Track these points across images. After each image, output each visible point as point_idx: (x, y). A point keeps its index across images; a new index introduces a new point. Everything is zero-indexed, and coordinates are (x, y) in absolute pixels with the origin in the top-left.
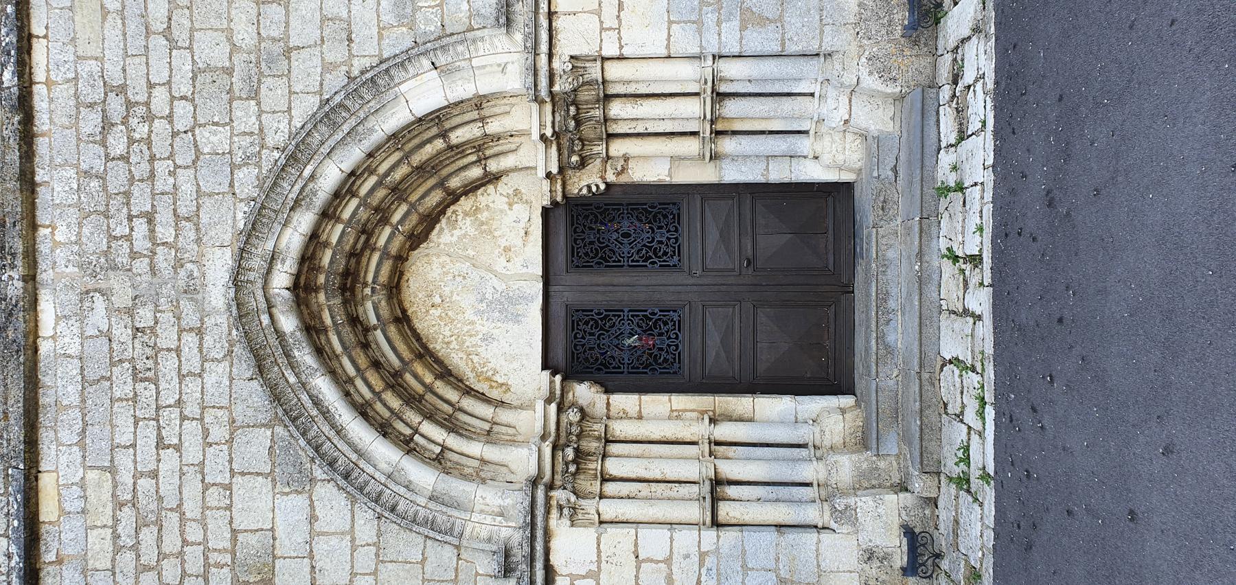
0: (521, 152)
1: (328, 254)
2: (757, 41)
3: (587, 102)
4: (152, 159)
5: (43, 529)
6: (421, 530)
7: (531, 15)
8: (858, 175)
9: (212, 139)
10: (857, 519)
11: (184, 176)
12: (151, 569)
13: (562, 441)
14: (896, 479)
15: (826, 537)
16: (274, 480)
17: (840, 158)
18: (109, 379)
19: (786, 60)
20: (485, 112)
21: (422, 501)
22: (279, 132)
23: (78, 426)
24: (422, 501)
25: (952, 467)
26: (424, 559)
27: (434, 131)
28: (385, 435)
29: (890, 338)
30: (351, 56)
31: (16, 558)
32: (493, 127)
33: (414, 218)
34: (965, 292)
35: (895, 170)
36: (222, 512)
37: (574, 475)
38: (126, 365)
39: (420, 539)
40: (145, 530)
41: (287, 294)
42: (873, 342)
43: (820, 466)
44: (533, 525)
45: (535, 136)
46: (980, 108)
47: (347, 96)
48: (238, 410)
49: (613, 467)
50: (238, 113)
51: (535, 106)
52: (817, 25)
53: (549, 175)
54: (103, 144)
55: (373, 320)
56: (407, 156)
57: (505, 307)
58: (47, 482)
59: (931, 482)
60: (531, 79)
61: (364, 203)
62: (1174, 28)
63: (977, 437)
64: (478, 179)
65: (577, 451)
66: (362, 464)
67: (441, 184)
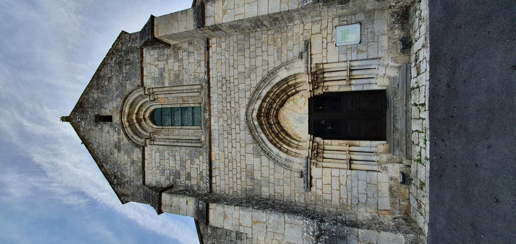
0: (303, 86)
1: (264, 109)
2: (361, 56)
3: (319, 74)
4: (230, 91)
5: (212, 162)
6: (283, 166)
7: (307, 55)
8: (387, 87)
9: (242, 86)
10: (388, 170)
11: (236, 94)
12: (231, 171)
13: (313, 149)
14: (398, 160)
15: (379, 173)
16: (253, 155)
17: (383, 83)
18: (223, 134)
19: (369, 60)
20: (296, 78)
21: (283, 160)
22: (254, 84)
23: (218, 143)
24: (283, 160)
25: (415, 157)
26: (284, 173)
27: (285, 82)
28: (275, 147)
29: (397, 126)
30: (268, 67)
31: (208, 167)
32: (298, 81)
33: (281, 101)
34: (419, 113)
35: (398, 85)
36: (244, 161)
37: (316, 157)
38: (226, 131)
39: (283, 168)
40: (230, 163)
41: (256, 117)
42: (392, 127)
43: (378, 157)
44: (307, 167)
45: (307, 82)
46: (425, 66)
47: (268, 76)
48: (247, 140)
49: (325, 155)
50: (246, 81)
51: (307, 75)
52: (377, 51)
53: (310, 91)
54: (222, 88)
55: (273, 123)
56: (280, 88)
57: (300, 120)
58: (213, 153)
59: (409, 161)
60: (306, 69)
61: (271, 98)
62: (489, 33)
63: (424, 149)
64: (294, 92)
65: (317, 151)
66: (271, 152)
67: (286, 94)
